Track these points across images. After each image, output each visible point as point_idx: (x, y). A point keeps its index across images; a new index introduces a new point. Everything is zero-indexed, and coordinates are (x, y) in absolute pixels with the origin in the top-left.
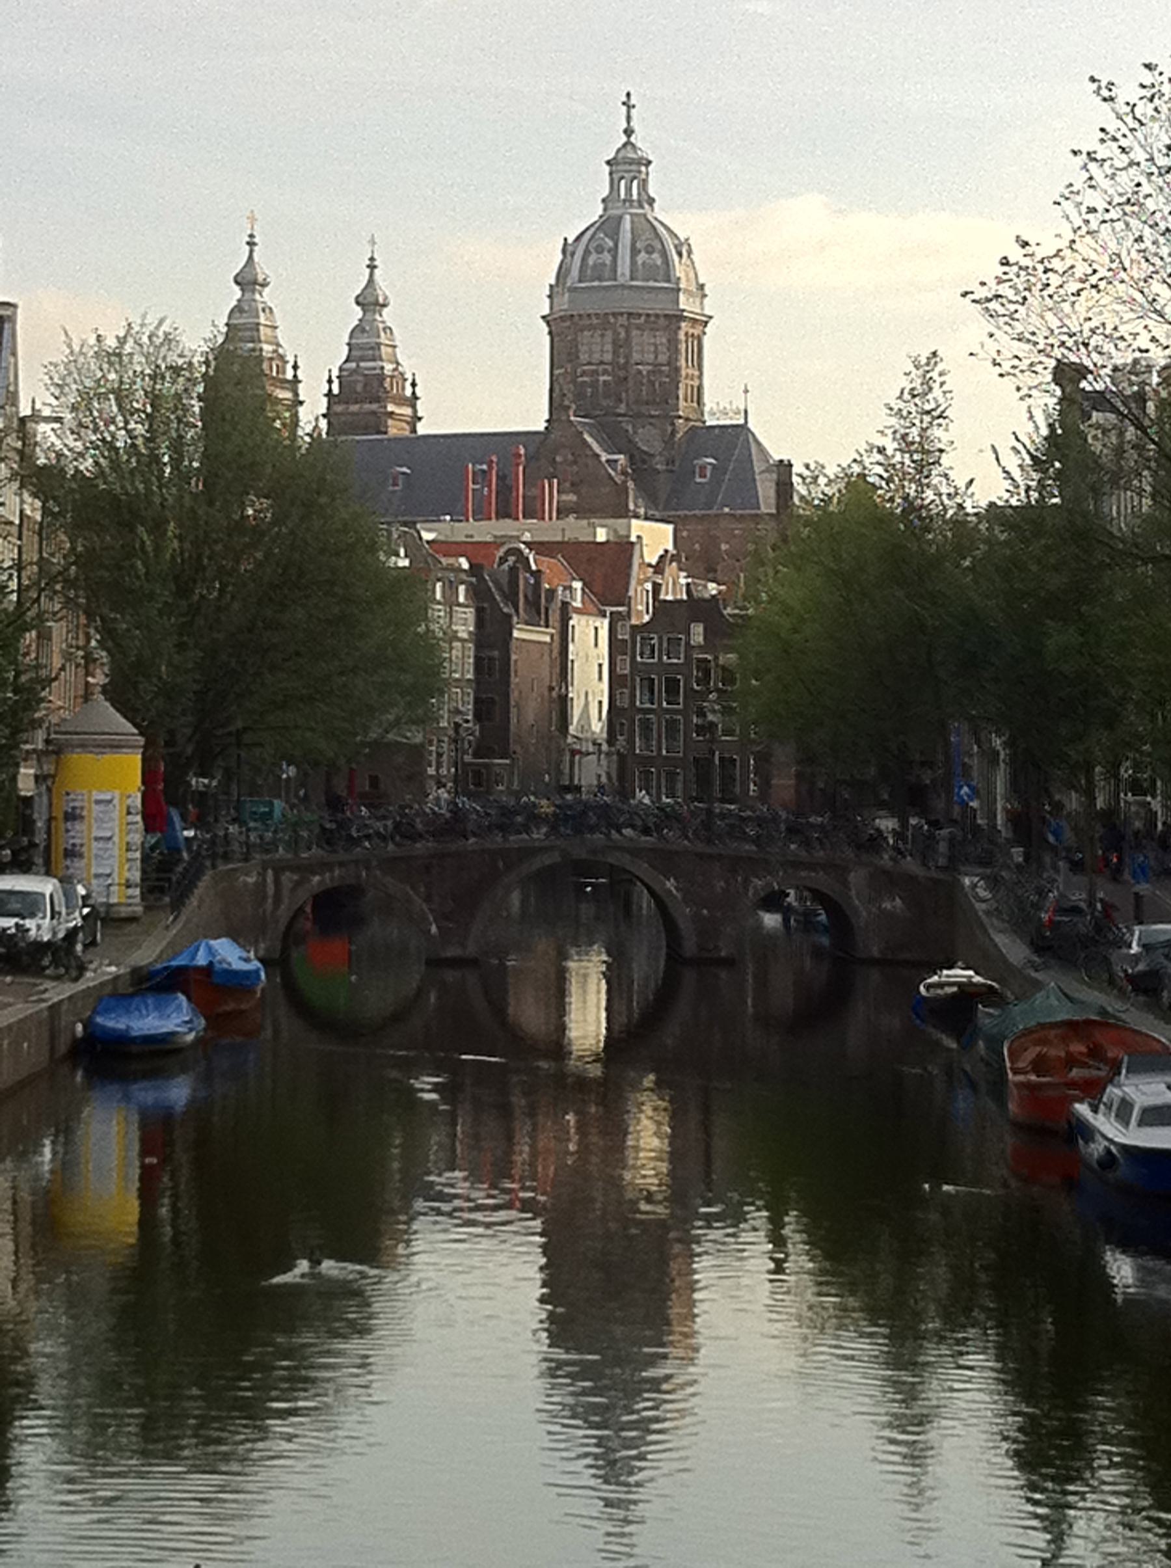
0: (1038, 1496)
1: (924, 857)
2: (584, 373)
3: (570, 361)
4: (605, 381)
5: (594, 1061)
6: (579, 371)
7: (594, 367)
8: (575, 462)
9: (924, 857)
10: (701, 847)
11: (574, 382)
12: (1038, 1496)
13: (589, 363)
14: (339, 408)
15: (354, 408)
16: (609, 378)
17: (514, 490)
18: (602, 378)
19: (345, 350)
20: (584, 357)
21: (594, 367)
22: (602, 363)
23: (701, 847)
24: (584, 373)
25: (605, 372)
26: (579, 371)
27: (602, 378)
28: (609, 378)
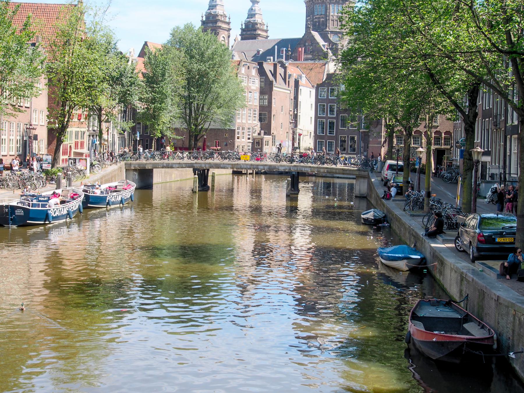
0: (302, 329)
1: (468, 169)
2: (316, 18)
3: (312, 14)
4: (322, 21)
5: (39, 305)
6: (314, 18)
7: (319, 16)
8: (312, 45)
9: (468, 169)
10: (331, 180)
11: (313, 21)
12: (302, 329)
13: (318, 15)
14: (244, 33)
15: (249, 33)
16: (324, 19)
17: (184, 295)
18: (322, 20)
19: (247, 15)
20: (316, 13)
21: (319, 16)
22: (321, 15)
23: (331, 180)
24: (316, 18)
25: (322, 18)
26: (314, 18)
27: (322, 20)
28: (324, 19)
